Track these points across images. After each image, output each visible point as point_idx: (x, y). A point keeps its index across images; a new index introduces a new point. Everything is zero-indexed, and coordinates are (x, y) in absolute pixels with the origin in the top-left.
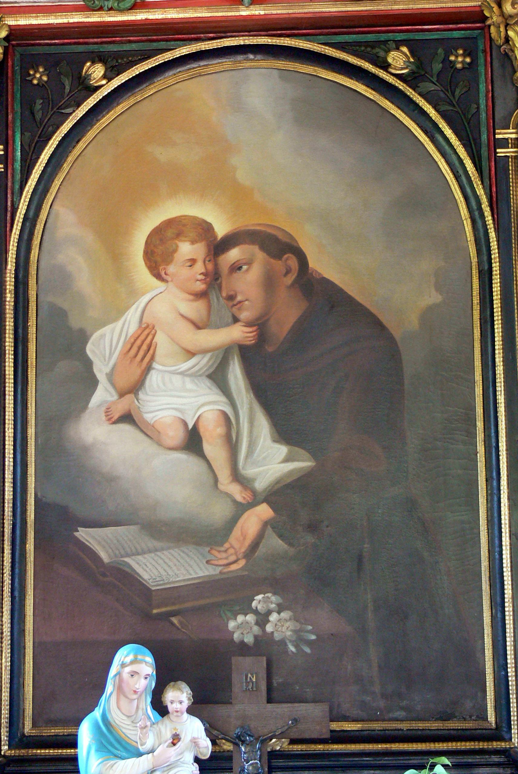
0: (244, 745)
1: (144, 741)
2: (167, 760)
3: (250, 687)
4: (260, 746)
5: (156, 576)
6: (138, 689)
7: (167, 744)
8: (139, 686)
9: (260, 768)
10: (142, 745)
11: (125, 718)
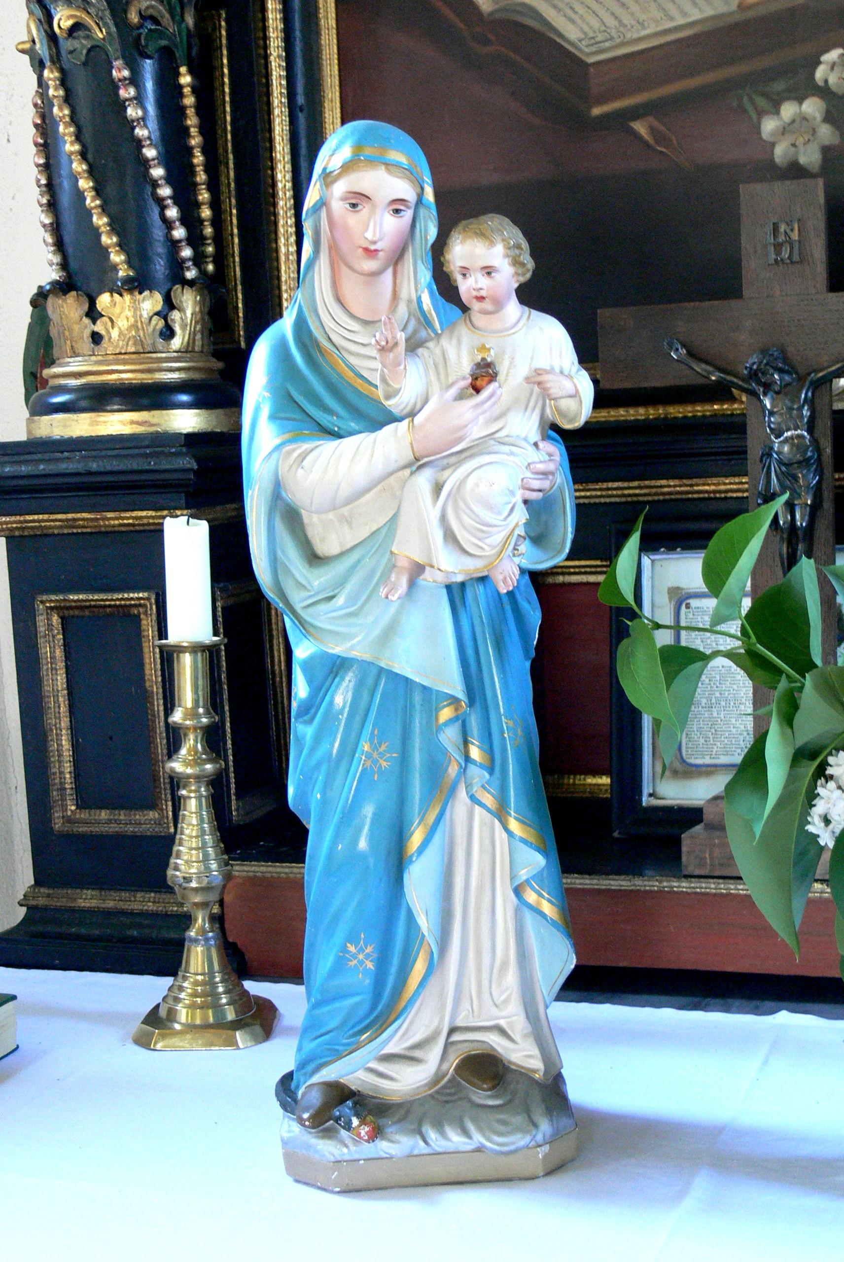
0: (769, 396)
1: (396, 386)
2: (460, 434)
3: (785, 254)
4: (810, 394)
5: (595, 32)
6: (374, 243)
7: (453, 392)
8: (374, 235)
9: (808, 447)
10: (388, 397)
11: (354, 326)
